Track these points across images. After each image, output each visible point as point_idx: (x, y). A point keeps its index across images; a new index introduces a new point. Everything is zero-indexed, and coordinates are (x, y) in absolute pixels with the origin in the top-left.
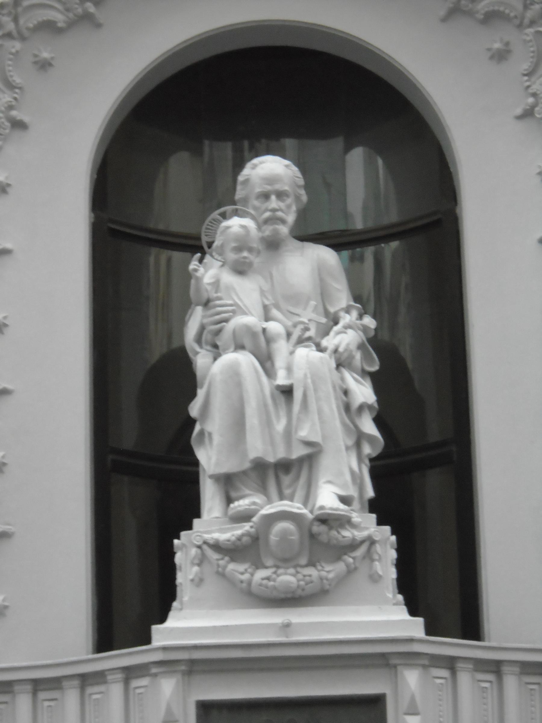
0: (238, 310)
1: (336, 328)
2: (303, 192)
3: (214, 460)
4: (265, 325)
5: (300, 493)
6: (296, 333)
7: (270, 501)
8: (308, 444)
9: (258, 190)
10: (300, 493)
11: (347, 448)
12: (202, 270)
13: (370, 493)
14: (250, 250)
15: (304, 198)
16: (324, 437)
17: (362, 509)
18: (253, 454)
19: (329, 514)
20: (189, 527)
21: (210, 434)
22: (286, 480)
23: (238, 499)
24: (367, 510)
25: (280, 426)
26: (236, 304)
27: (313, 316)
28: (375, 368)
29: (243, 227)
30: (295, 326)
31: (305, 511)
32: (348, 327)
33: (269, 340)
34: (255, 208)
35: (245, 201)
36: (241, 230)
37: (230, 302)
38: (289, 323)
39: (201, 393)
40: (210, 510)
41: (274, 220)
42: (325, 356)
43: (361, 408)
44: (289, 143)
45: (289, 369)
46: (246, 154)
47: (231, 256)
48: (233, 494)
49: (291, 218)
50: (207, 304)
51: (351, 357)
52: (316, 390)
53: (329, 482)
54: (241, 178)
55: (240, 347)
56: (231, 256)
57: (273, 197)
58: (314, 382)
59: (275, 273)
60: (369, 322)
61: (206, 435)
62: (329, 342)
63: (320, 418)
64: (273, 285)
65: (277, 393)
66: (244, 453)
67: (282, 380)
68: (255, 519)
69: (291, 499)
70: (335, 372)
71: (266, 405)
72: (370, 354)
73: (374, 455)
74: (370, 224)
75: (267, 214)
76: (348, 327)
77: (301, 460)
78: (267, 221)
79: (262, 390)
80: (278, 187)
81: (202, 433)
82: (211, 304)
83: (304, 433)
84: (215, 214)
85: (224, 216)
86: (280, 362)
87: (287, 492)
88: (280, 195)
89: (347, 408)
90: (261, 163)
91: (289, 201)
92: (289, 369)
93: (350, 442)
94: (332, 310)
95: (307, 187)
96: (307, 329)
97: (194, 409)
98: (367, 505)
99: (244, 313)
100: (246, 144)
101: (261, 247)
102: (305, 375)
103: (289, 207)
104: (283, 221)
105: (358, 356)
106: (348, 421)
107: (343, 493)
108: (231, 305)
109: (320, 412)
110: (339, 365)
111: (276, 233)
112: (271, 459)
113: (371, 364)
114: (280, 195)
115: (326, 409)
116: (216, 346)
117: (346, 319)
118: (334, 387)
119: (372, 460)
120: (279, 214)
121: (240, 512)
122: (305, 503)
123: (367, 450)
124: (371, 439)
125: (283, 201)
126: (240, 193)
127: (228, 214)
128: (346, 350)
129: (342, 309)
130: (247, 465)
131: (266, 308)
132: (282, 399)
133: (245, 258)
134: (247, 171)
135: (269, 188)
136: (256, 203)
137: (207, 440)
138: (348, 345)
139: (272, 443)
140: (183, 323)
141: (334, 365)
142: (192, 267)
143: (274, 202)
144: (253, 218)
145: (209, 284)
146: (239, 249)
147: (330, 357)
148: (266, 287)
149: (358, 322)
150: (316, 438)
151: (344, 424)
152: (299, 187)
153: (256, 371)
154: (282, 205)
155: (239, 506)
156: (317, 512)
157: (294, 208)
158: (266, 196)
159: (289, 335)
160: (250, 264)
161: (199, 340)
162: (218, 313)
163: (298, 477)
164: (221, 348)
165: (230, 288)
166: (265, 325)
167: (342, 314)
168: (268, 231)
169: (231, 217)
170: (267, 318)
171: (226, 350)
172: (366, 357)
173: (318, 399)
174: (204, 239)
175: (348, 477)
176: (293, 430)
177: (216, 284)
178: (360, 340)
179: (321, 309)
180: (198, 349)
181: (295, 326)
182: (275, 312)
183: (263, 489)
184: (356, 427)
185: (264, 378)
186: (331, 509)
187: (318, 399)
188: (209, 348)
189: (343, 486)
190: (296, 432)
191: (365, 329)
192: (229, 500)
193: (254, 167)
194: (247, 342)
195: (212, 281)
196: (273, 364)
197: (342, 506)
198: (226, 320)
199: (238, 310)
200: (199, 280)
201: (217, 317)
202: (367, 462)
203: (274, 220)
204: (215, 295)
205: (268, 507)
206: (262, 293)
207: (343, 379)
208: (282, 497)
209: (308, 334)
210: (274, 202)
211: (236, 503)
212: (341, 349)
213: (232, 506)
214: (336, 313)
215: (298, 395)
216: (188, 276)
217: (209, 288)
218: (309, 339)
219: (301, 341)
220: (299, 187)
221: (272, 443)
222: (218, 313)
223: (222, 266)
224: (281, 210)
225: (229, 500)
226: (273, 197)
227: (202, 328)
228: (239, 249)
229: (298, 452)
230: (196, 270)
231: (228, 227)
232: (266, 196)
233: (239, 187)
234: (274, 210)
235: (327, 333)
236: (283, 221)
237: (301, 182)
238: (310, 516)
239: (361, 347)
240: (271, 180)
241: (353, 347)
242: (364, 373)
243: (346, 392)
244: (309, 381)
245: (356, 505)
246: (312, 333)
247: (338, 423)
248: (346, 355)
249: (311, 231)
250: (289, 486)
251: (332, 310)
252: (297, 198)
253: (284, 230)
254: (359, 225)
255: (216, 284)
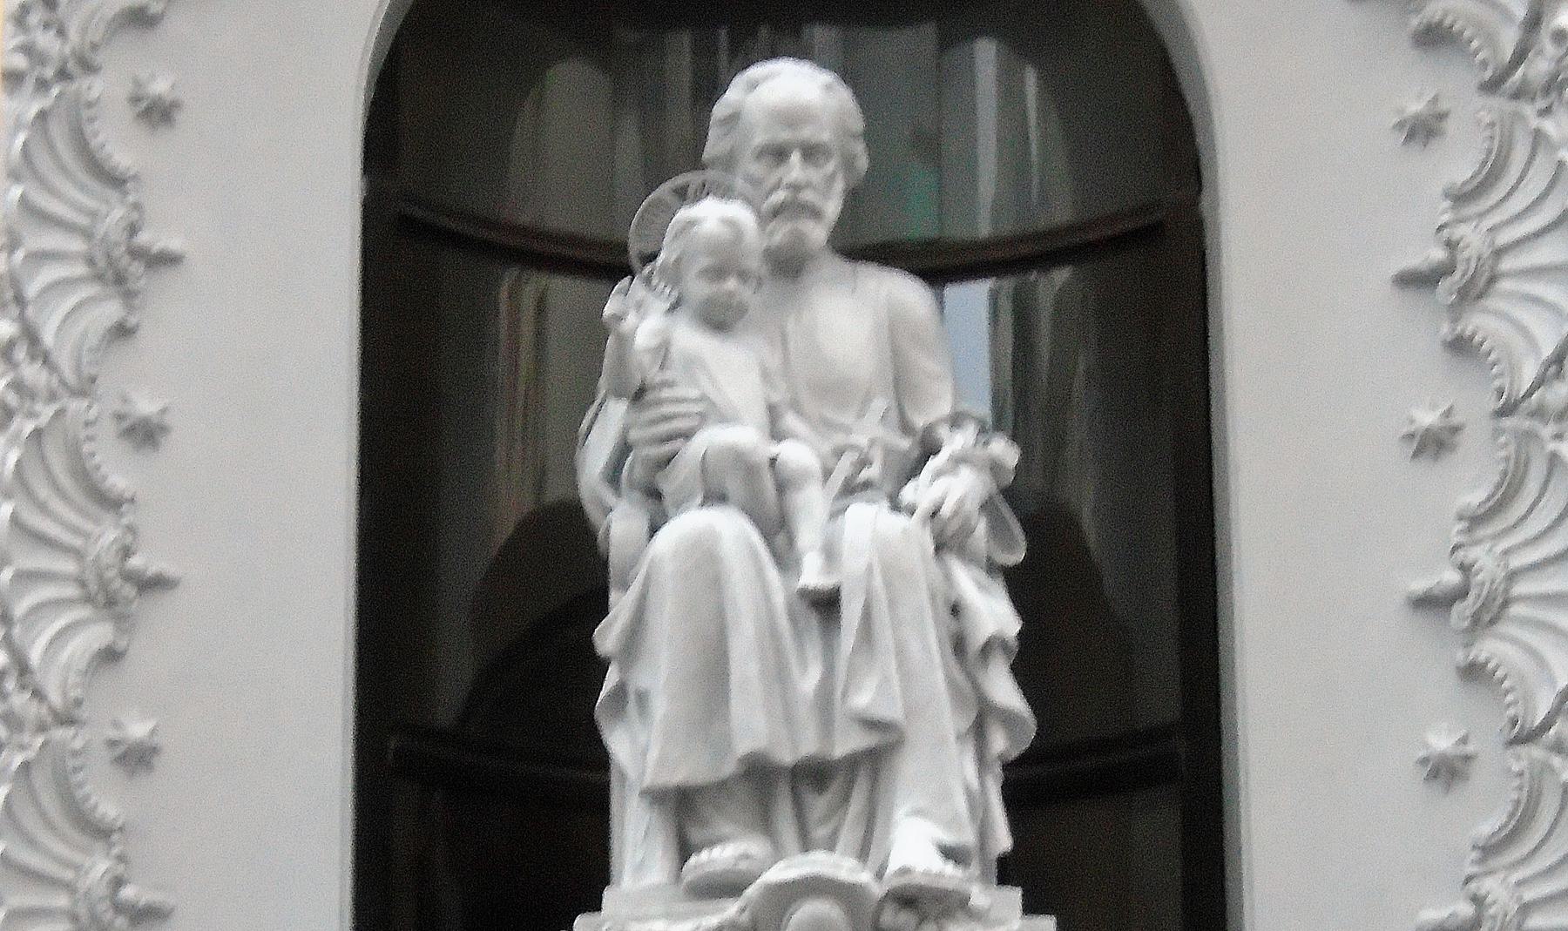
0: (712, 413)
1: (933, 463)
2: (859, 148)
3: (653, 754)
4: (774, 449)
5: (849, 834)
6: (843, 468)
7: (778, 854)
8: (872, 725)
9: (759, 139)
10: (849, 834)
11: (959, 737)
12: (631, 319)
13: (1003, 840)
14: (743, 276)
15: (863, 163)
16: (909, 710)
17: (984, 877)
18: (744, 745)
19: (921, 888)
20: (596, 906)
21: (642, 698)
22: (818, 805)
23: (711, 843)
24: (995, 880)
25: (808, 681)
26: (703, 398)
27: (879, 432)
28: (1017, 556)
29: (731, 223)
30: (839, 453)
31: (864, 877)
32: (958, 461)
33: (784, 485)
34: (755, 182)
35: (728, 162)
36: (724, 232)
37: (693, 393)
38: (826, 448)
39: (621, 605)
40: (640, 868)
41: (794, 209)
42: (900, 521)
43: (987, 649)
44: (820, 34)
45: (830, 554)
46: (723, 57)
47: (698, 289)
48: (695, 835)
49: (832, 208)
50: (639, 396)
51: (966, 531)
52: (892, 604)
53: (918, 812)
54: (720, 110)
55: (715, 497)
56: (698, 289)
57: (795, 157)
58: (888, 585)
59: (791, 326)
60: (1005, 451)
61: (632, 697)
62: (919, 492)
63: (900, 665)
64: (786, 360)
65: (802, 608)
66: (722, 744)
67: (813, 575)
68: (751, 891)
69: (830, 845)
70: (933, 566)
71: (774, 634)
72: (1003, 520)
73: (1014, 754)
74: (1008, 228)
75: (780, 196)
76: (958, 461)
77: (853, 763)
78: (776, 212)
79: (767, 597)
80: (807, 133)
81: (620, 692)
82: (649, 397)
83: (864, 699)
84: (664, 190)
85: (682, 195)
86: (808, 536)
87: (820, 833)
88: (812, 153)
89: (959, 645)
90: (766, 78)
91: (831, 166)
92: (830, 554)
93: (966, 722)
94: (920, 422)
95: (871, 136)
96: (864, 463)
97: (607, 637)
98: (994, 870)
99: (724, 419)
100: (723, 34)
101: (765, 271)
102: (870, 569)
103: (831, 179)
104: (815, 213)
105: (981, 527)
106: (960, 677)
107: (949, 839)
108: (696, 401)
109: (901, 652)
110: (940, 548)
111: (799, 238)
112: (786, 757)
113: (1010, 547)
114: (812, 153)
115: (914, 647)
116: (655, 494)
117: (956, 442)
118: (933, 597)
119: (1008, 767)
120: (808, 196)
121: (708, 876)
122: (863, 853)
123: (1000, 743)
124: (1008, 719)
125: (817, 166)
126: (714, 145)
127: (691, 191)
128: (956, 513)
129: (942, 421)
130: (729, 768)
131: (773, 413)
132: (813, 621)
133: (731, 294)
134: (735, 94)
135: (784, 136)
136: (756, 168)
137: (632, 706)
138: (961, 502)
139: (789, 718)
140: (572, 441)
141: (931, 548)
142: (609, 310)
143: (795, 169)
144: (749, 201)
145: (649, 351)
146: (718, 273)
147: (924, 524)
148: (774, 361)
149: (979, 452)
150: (891, 711)
151: (951, 683)
152: (854, 136)
153: (755, 556)
154: (815, 175)
155: (711, 861)
156: (891, 881)
157: (839, 186)
158: (778, 154)
159: (827, 473)
160: (741, 310)
161: (613, 475)
162: (667, 418)
163: (846, 799)
164: (668, 501)
165: (693, 364)
166: (774, 449)
167: (943, 432)
168: (781, 233)
169: (697, 199)
170: (777, 435)
171: (680, 505)
172: (997, 529)
173: (896, 625)
174: (635, 248)
175: (961, 803)
176: (838, 694)
177: (663, 351)
178: (985, 496)
179: (894, 415)
180: (609, 497)
181: (839, 453)
182: (790, 421)
183: (764, 823)
184: (976, 687)
185: (772, 573)
186: (926, 874)
187: (896, 625)
188: (637, 495)
189: (951, 823)
190: (845, 694)
191: (995, 467)
192: (685, 850)
193: (753, 85)
194: (733, 486)
195: (654, 343)
196: (791, 541)
197: (950, 869)
198: (687, 435)
199: (712, 413)
200: (625, 341)
201: (664, 428)
202: (998, 770)
203: (794, 209)
204: (658, 379)
205: (781, 864)
206: (766, 375)
207: (948, 577)
208: (806, 845)
209: (865, 474)
210: (795, 169)
211: (704, 856)
212: (946, 511)
213: (693, 860)
214: (929, 430)
215: (851, 612)
216: (596, 333)
217: (646, 359)
218: (867, 485)
219: (851, 489)
220: (854, 136)
221: (789, 718)
222: (667, 418)
223: (673, 308)
224: (808, 185)
225: (685, 850)
226: (795, 157)
227: (624, 449)
228: (718, 273)
229: (848, 742)
230: (619, 318)
231: (691, 223)
232: (778, 154)
233: (713, 133)
234: (796, 188)
235: (914, 470)
236: (815, 213)
237: (857, 123)
238: (878, 890)
239: (987, 507)
240: (791, 117)
241: (972, 506)
242: (992, 568)
243: (956, 610)
244: (878, 582)
245: (975, 869)
246: (872, 472)
247: (939, 677)
248: (953, 527)
249: (875, 234)
250: (826, 819)
251: (920, 422)
252: (848, 163)
253: (818, 233)
254: (984, 230)
255: (663, 351)
